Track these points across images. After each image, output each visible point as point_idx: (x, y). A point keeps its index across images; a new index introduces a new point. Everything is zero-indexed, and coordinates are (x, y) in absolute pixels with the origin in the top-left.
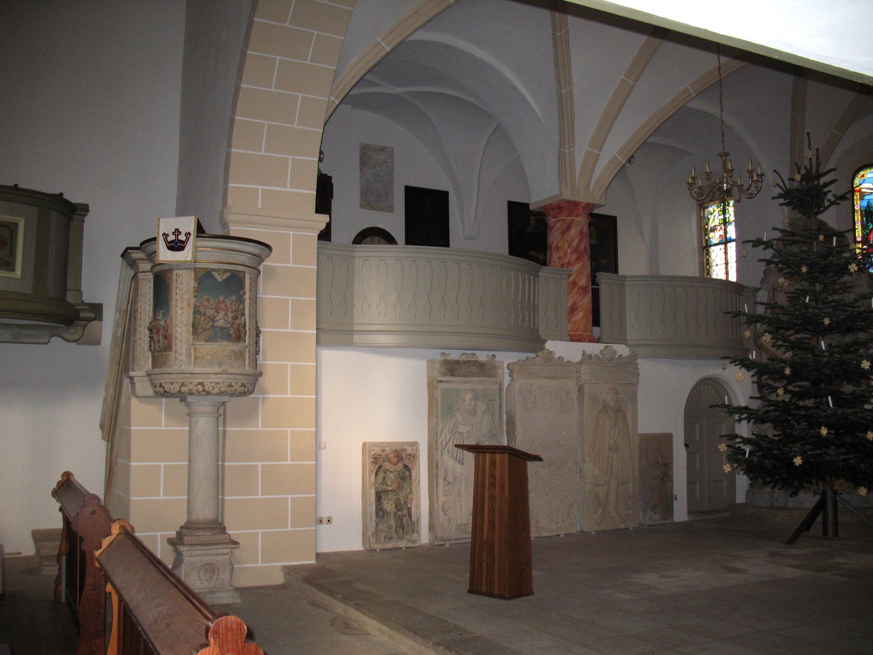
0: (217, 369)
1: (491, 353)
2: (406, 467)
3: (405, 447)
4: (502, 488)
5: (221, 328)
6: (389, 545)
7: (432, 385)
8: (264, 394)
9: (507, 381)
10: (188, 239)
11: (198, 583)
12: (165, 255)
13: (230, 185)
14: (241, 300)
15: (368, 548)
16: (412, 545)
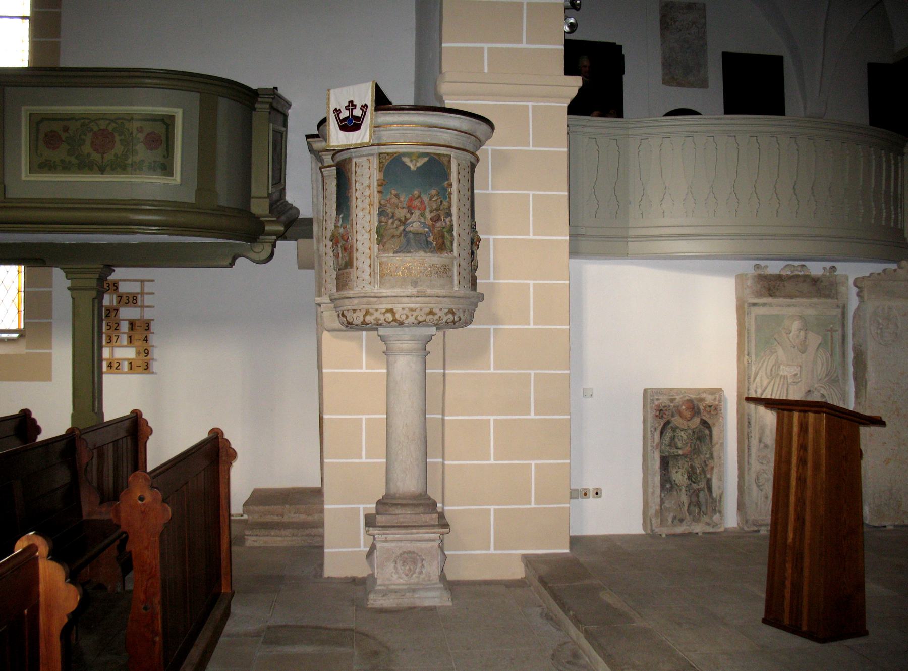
0: (410, 290)
1: (828, 264)
2: (704, 423)
3: (704, 395)
4: (816, 467)
5: (416, 234)
6: (680, 529)
7: (742, 309)
8: (496, 322)
9: (853, 303)
10: (364, 113)
11: (395, 576)
12: (338, 138)
13: (444, 45)
14: (445, 194)
15: (649, 532)
16: (711, 530)
